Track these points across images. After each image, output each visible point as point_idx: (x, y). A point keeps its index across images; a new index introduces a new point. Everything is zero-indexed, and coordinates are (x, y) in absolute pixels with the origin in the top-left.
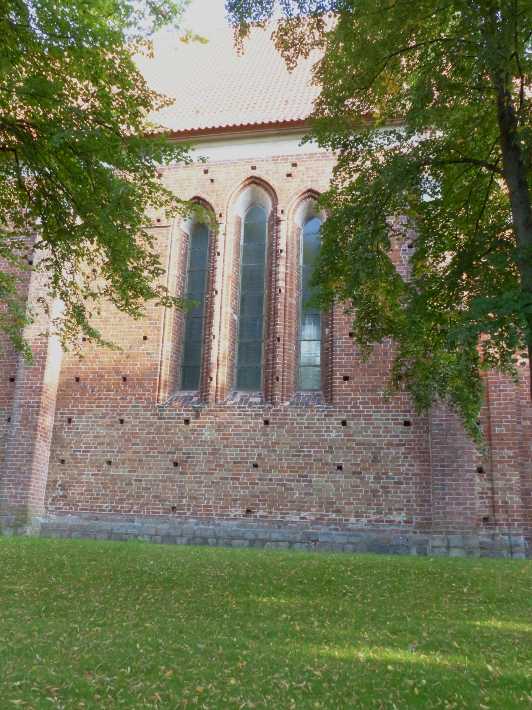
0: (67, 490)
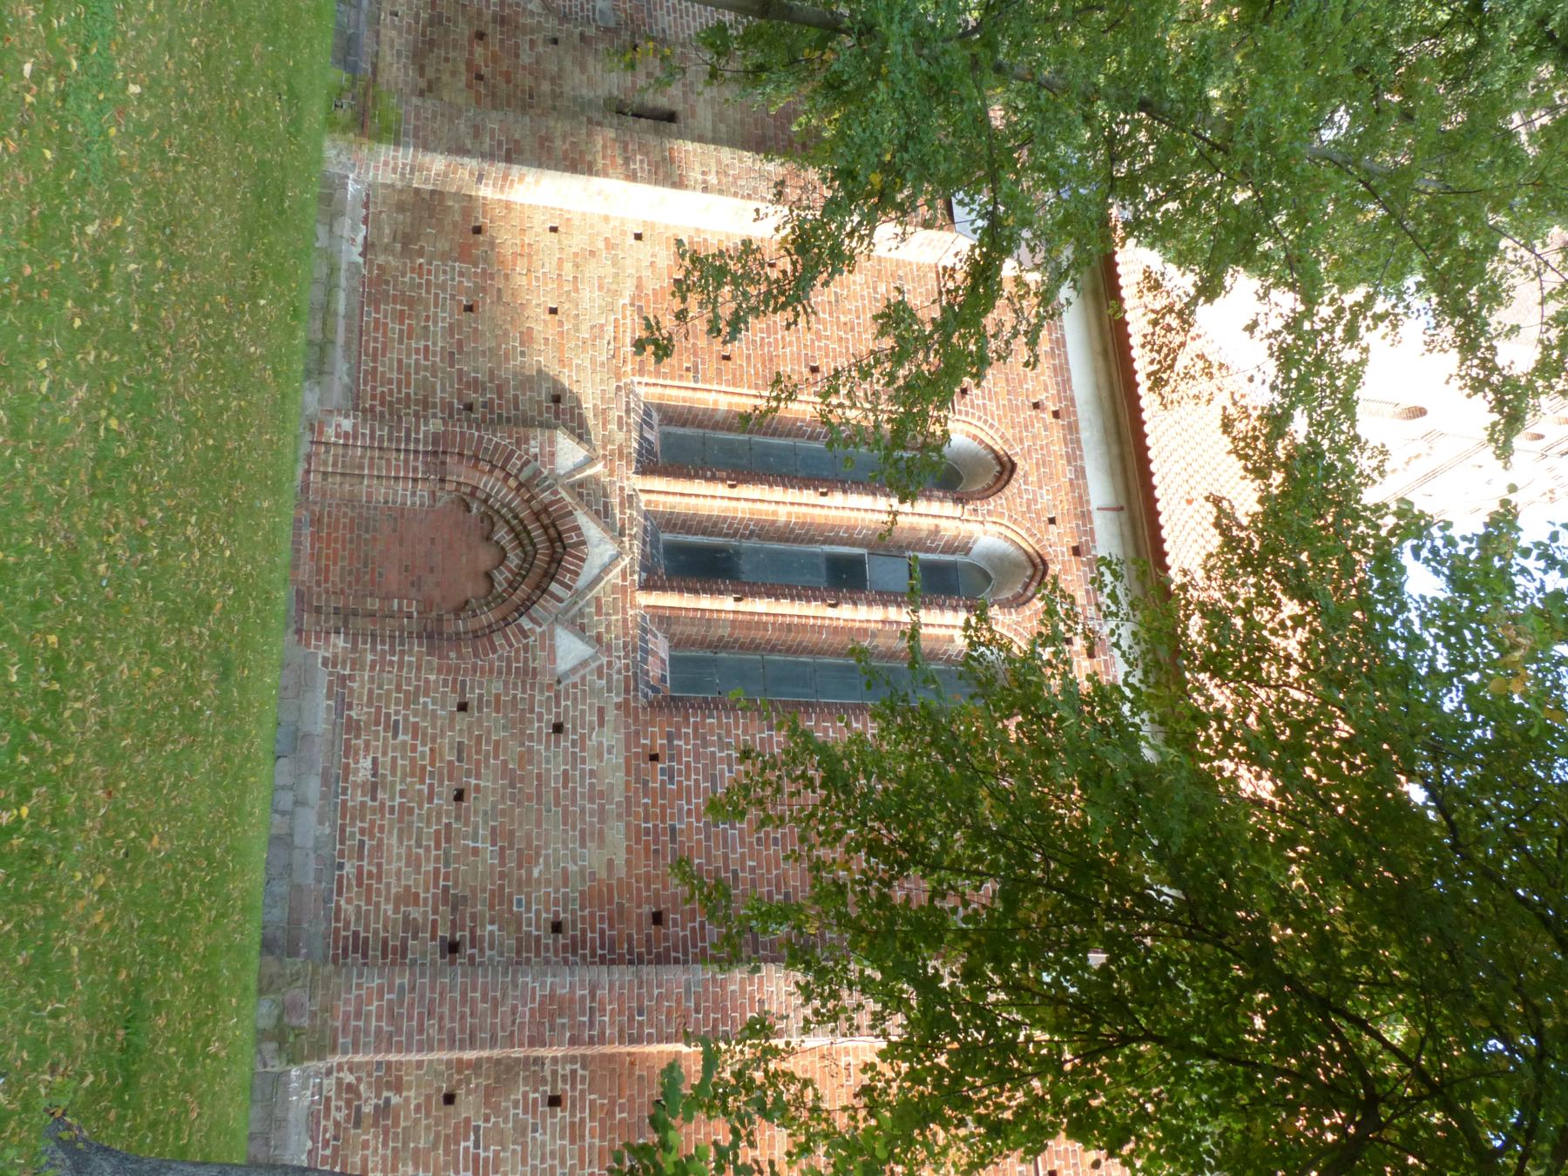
0: (376, 1124)
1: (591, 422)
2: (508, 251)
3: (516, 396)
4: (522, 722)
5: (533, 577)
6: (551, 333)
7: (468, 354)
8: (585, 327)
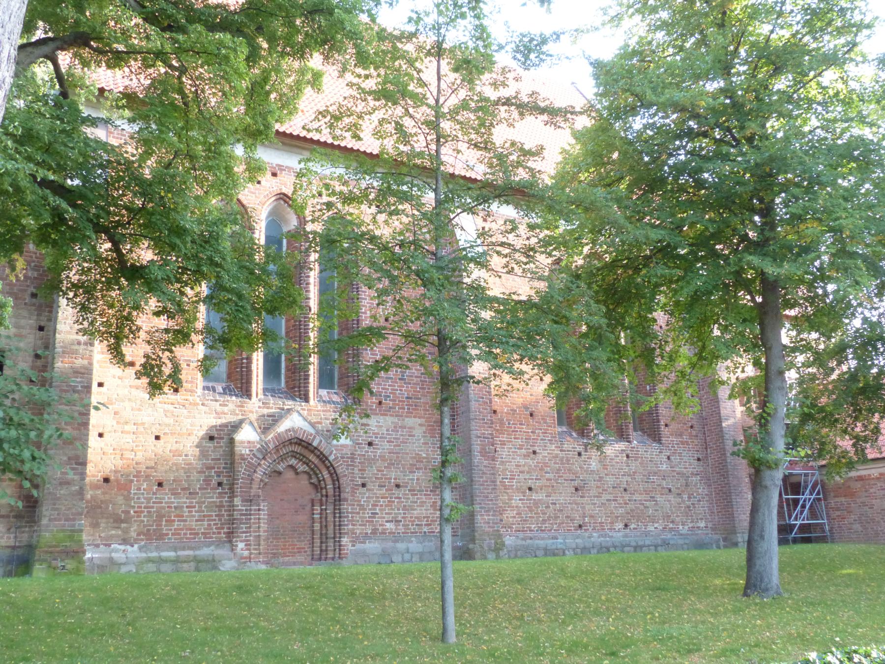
1: (224, 421)
2: (119, 463)
3: (212, 460)
4: (369, 460)
5: (306, 453)
6: (172, 440)
7: (189, 485)
8: (167, 421)
